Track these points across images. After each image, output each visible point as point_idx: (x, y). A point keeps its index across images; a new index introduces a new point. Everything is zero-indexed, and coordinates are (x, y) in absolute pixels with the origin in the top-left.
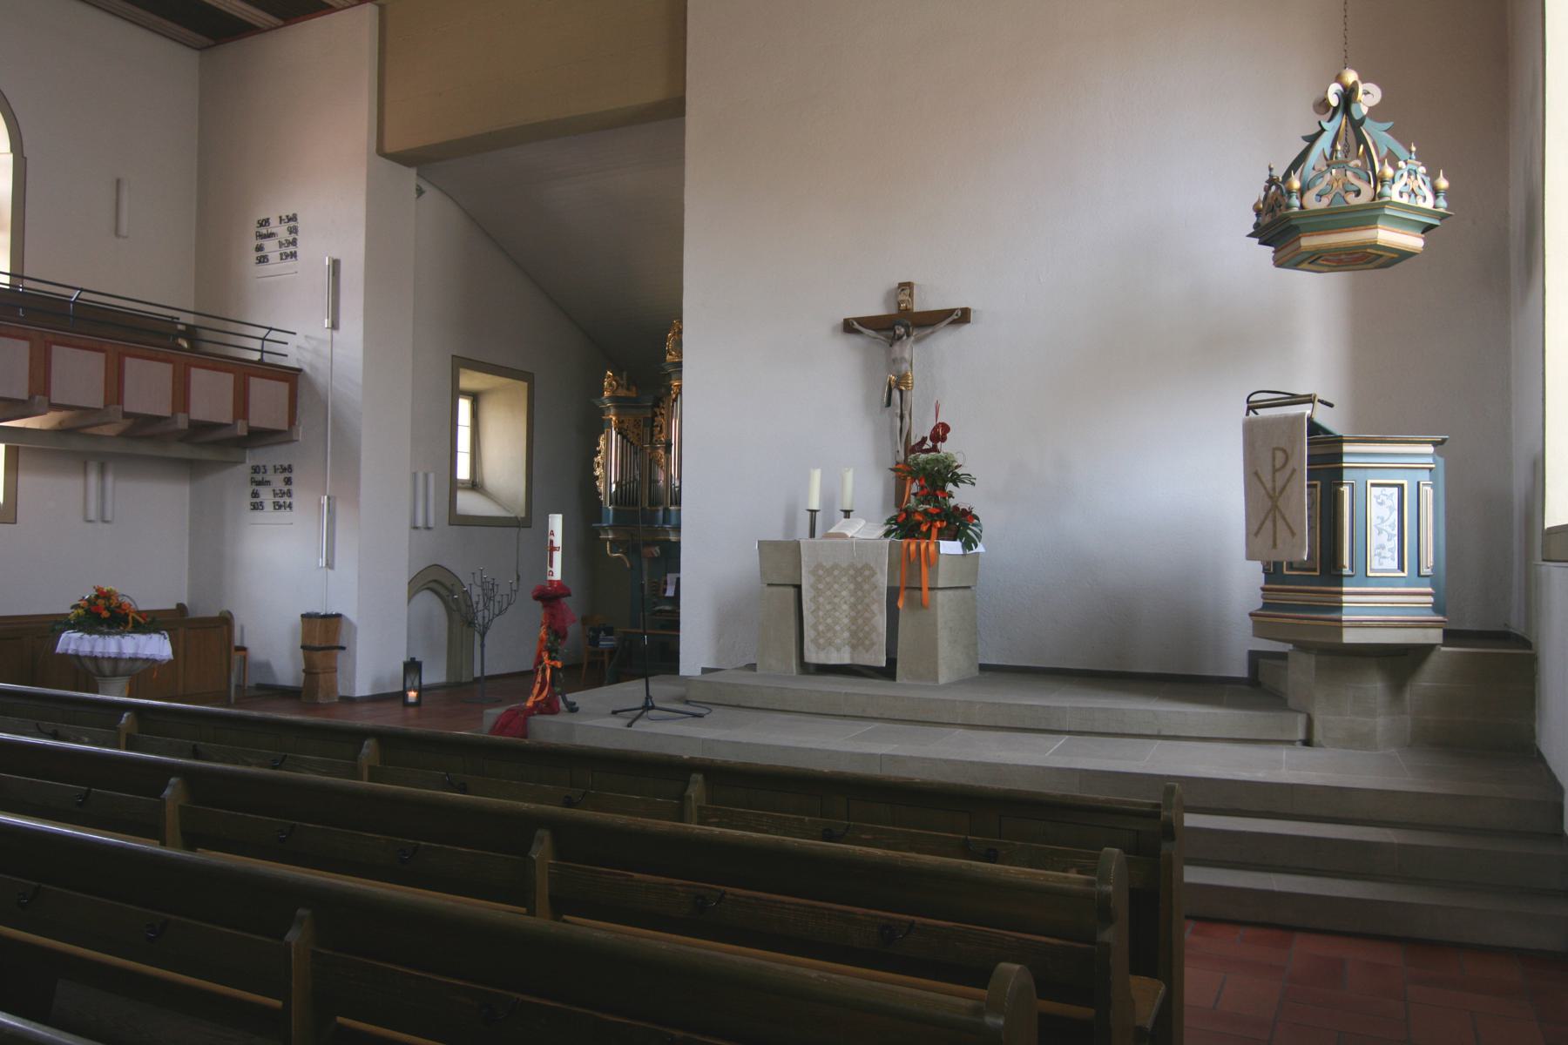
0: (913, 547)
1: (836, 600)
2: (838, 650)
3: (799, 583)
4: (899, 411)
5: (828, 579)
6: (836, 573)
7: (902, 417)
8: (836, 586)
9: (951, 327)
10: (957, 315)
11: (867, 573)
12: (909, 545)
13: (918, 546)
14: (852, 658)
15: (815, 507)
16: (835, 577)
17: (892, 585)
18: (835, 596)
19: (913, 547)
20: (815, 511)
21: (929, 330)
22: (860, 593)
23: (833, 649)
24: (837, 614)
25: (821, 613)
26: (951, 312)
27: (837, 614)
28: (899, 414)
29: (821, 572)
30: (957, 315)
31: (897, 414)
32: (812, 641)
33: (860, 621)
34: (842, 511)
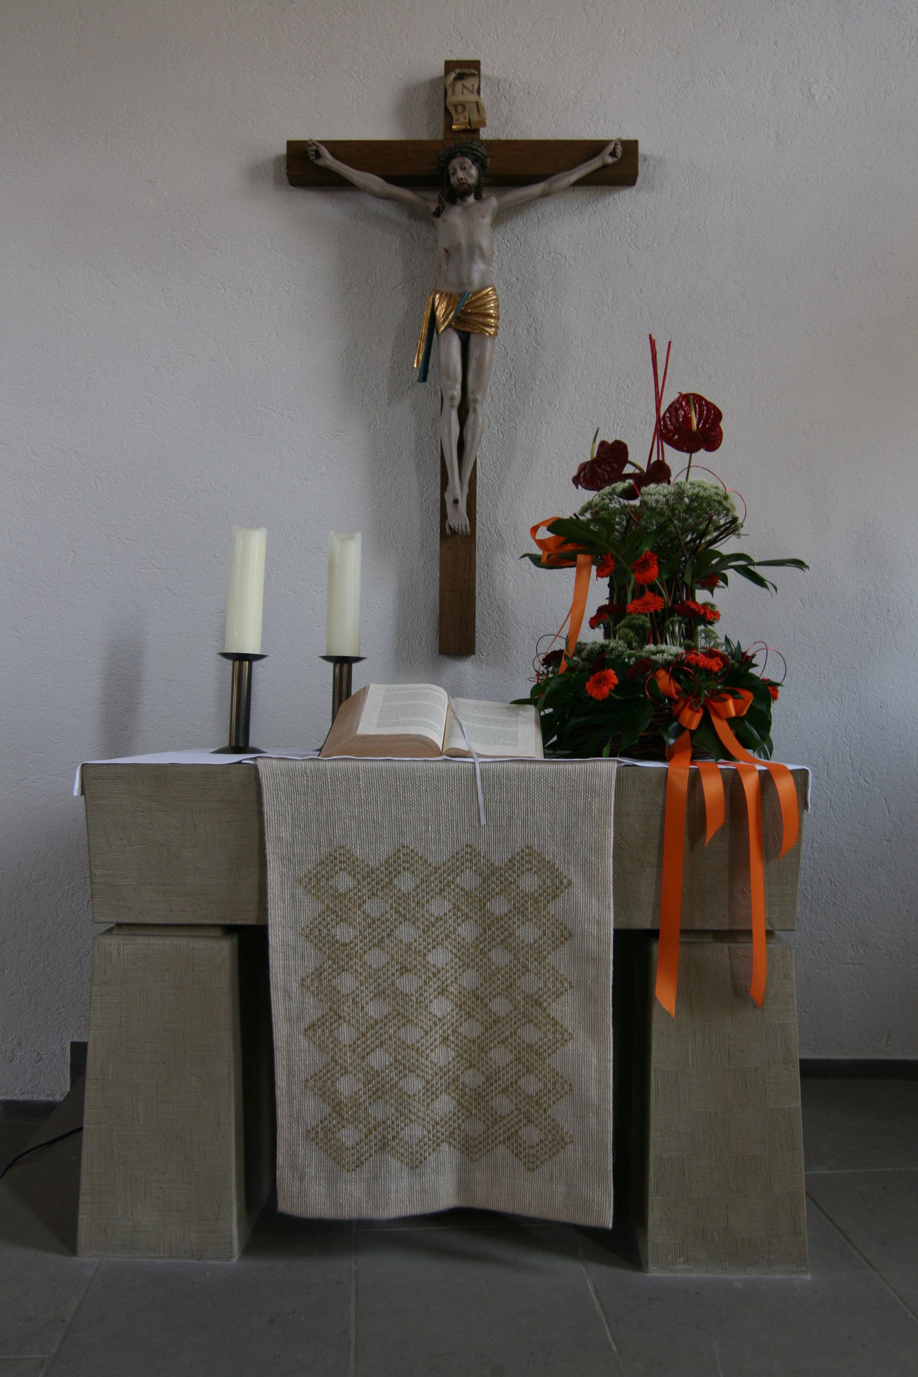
0: (713, 787)
1: (408, 984)
2: (415, 1164)
3: (250, 920)
4: (457, 392)
5: (373, 908)
6: (405, 883)
7: (464, 411)
8: (406, 933)
9: (582, 194)
10: (613, 154)
11: (529, 883)
12: (695, 780)
13: (733, 784)
14: (463, 1185)
15: (251, 646)
16: (405, 898)
17: (622, 926)
18: (404, 970)
19: (713, 787)
20: (251, 658)
21: (537, 189)
22: (499, 957)
23: (395, 1164)
24: (412, 1035)
25: (346, 1034)
26: (595, 148)
27: (412, 1035)
28: (457, 402)
29: (344, 882)
30: (613, 154)
31: (452, 398)
32: (310, 1135)
33: (500, 1056)
34: (328, 658)
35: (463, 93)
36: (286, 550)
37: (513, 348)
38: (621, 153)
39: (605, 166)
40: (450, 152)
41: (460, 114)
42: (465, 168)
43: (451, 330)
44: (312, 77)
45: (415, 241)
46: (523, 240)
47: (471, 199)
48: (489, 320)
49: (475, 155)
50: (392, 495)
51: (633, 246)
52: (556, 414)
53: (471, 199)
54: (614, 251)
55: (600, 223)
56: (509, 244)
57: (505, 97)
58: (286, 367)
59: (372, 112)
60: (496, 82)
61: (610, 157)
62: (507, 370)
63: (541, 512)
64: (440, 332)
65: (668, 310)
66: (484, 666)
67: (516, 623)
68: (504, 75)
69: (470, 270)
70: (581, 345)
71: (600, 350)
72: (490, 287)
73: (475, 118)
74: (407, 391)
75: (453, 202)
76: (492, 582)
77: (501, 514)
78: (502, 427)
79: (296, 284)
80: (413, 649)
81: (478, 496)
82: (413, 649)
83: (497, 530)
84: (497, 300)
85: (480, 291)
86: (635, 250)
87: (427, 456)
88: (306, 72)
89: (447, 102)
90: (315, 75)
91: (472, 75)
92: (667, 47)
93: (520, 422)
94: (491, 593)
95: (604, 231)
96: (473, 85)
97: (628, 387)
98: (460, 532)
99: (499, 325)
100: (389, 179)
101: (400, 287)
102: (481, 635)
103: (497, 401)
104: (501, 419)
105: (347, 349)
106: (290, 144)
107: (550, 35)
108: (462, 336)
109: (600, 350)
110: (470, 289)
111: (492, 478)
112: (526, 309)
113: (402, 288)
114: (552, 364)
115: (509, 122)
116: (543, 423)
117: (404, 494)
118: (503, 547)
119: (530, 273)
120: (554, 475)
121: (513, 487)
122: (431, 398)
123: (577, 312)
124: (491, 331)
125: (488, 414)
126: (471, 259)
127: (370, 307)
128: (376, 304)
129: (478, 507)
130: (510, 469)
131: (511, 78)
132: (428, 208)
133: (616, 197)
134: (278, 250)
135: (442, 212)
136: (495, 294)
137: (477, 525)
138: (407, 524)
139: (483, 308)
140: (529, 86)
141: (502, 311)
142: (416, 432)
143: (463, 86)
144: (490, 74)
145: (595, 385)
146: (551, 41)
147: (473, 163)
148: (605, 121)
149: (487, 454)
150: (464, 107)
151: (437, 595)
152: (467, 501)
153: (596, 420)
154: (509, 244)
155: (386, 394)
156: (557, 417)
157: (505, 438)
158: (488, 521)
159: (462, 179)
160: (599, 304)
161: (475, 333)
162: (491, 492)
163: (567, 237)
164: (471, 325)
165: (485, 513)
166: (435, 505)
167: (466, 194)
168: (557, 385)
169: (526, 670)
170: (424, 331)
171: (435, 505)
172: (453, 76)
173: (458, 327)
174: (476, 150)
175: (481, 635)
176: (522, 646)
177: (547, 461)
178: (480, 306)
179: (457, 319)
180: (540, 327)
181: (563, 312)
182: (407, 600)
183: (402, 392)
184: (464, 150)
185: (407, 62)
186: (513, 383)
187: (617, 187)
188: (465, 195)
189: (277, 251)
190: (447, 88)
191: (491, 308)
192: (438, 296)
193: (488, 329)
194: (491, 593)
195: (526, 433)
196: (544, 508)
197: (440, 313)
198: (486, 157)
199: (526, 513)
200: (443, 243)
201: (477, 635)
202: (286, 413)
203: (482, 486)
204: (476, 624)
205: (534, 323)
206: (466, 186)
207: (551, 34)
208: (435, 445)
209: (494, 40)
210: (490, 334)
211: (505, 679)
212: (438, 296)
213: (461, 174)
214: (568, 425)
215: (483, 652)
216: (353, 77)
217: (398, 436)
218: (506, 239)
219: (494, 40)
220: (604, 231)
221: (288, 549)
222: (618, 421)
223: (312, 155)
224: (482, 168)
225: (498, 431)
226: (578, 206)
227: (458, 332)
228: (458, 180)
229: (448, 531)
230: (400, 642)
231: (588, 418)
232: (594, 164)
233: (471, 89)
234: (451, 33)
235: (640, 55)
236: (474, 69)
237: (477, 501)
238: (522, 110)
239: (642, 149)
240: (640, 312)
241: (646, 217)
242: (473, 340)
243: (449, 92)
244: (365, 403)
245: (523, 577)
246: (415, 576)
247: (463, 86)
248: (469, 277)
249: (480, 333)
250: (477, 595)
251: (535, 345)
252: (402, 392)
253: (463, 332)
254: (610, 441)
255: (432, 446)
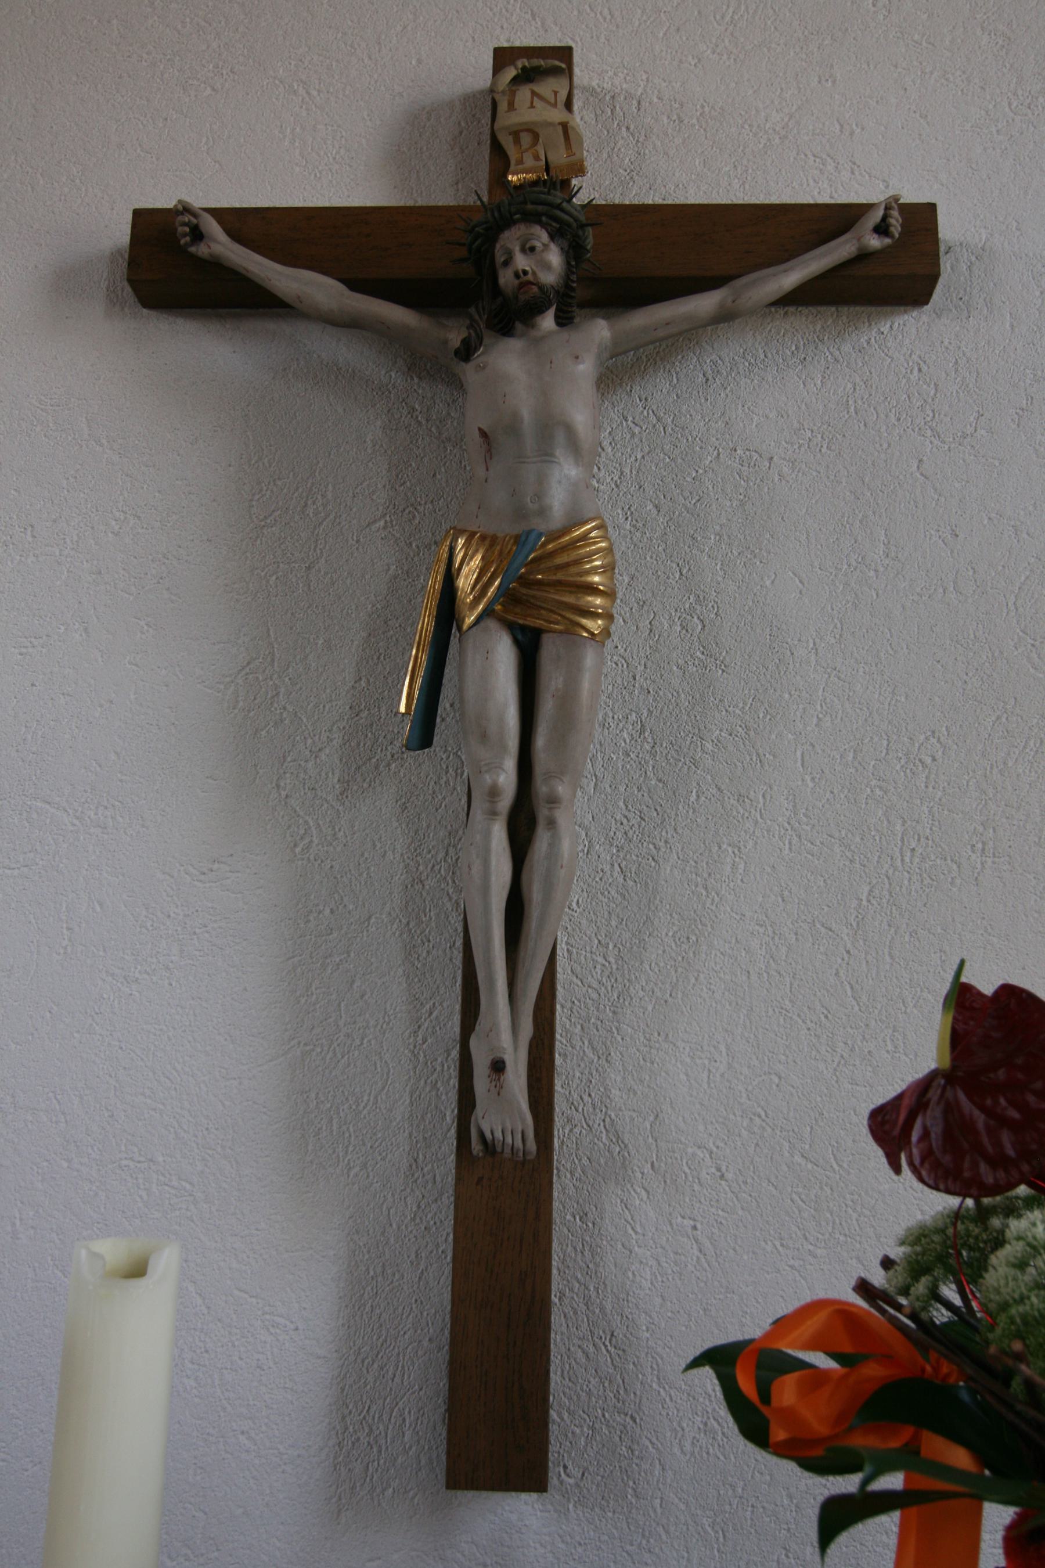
4: (507, 778)
10: (882, 229)
21: (705, 303)
28: (506, 801)
30: (882, 229)
31: (494, 793)
35: (532, 106)
36: (65, 1164)
37: (649, 663)
38: (900, 229)
39: (863, 256)
40: (496, 214)
41: (527, 150)
42: (532, 249)
43: (492, 624)
44: (209, 91)
45: (419, 423)
46: (670, 421)
47: (548, 322)
48: (590, 599)
49: (555, 219)
50: (341, 1023)
51: (929, 433)
52: (756, 823)
53: (548, 322)
54: (885, 446)
55: (850, 385)
56: (637, 430)
57: (628, 128)
58: (101, 706)
59: (334, 159)
60: (608, 98)
61: (876, 236)
62: (633, 717)
63: (722, 1076)
64: (465, 627)
65: (1023, 578)
66: (571, 1506)
67: (659, 1384)
68: (624, 86)
69: (542, 480)
70: (813, 658)
71: (861, 670)
72: (592, 519)
73: (559, 157)
74: (389, 765)
75: (506, 330)
76: (597, 1265)
77: (619, 1079)
78: (621, 855)
79: (139, 518)
80: (380, 1452)
81: (559, 1029)
82: (380, 1452)
83: (608, 1120)
84: (609, 550)
85: (566, 530)
86: (936, 442)
87: (433, 924)
88: (195, 82)
89: (496, 127)
90: (213, 89)
91: (555, 71)
92: (983, 29)
93: (666, 842)
94: (593, 1295)
95: (860, 402)
96: (556, 93)
97: (934, 759)
98: (507, 1150)
99: (614, 611)
100: (355, 285)
101: (382, 523)
102: (566, 1416)
103: (608, 790)
104: (619, 835)
105: (249, 663)
106: (140, 217)
107: (725, 7)
108: (520, 637)
109: (861, 670)
110: (541, 525)
111: (595, 985)
112: (677, 575)
113: (385, 528)
114: (745, 703)
115: (636, 178)
116: (724, 846)
117: (372, 1023)
118: (624, 1166)
119: (687, 494)
120: (754, 977)
121: (650, 1008)
122: (447, 782)
123: (801, 582)
124: (595, 625)
125: (586, 823)
126: (546, 455)
127: (309, 568)
128: (323, 560)
129: (558, 1060)
130: (642, 963)
131: (640, 90)
132: (446, 342)
133: (885, 329)
134: (104, 441)
135: (476, 349)
136: (605, 538)
137: (557, 1109)
138: (376, 1102)
139: (573, 570)
140: (682, 105)
141: (622, 581)
142: (407, 866)
143: (534, 93)
144: (594, 84)
145: (851, 755)
146: (728, 18)
147: (552, 237)
148: (853, 173)
149: (584, 921)
150: (536, 137)
151: (447, 1296)
152: (530, 1053)
153: (858, 839)
154: (637, 430)
155: (337, 771)
156: (758, 833)
157: (630, 883)
158: (586, 1098)
159: (525, 273)
160: (854, 563)
161: (554, 631)
162: (593, 1020)
163: (772, 415)
164: (543, 612)
165: (578, 1074)
166: (448, 1052)
167: (535, 309)
168: (758, 754)
169: (686, 1524)
170: (426, 623)
171: (448, 1052)
172: (511, 73)
173: (510, 617)
174: (559, 207)
175: (566, 1416)
176: (676, 1450)
177: (737, 941)
178: (568, 565)
179: (509, 597)
180: (713, 616)
181: (768, 583)
182: (368, 1308)
183: (377, 768)
184: (530, 207)
185: (414, 62)
186: (648, 747)
187: (889, 309)
188: (532, 310)
189: (101, 445)
190: (497, 97)
191: (594, 571)
192: (461, 542)
193: (585, 622)
194: (593, 1295)
195: (683, 871)
196: (730, 1066)
197: (465, 581)
198: (582, 226)
199: (683, 1077)
200: (478, 417)
201: (553, 1414)
202: (92, 814)
203: (569, 1005)
204: (552, 1385)
205: (698, 607)
206: (535, 289)
207: (728, 6)
208: (455, 897)
209: (605, 19)
210: (593, 634)
211: (628, 1548)
212: (461, 542)
213: (521, 262)
214: (787, 852)
215: (570, 1467)
216: (295, 92)
217: (361, 875)
218: (630, 419)
219: (605, 19)
220: (860, 402)
221: (69, 1161)
222: (913, 845)
223: (185, 235)
224: (574, 252)
225: (612, 865)
226: (797, 348)
227: (512, 628)
228: (517, 275)
229: (476, 1147)
230: (346, 1428)
231: (837, 835)
232: (841, 250)
233: (553, 101)
234: (510, 7)
235: (924, 44)
236: (561, 61)
237: (558, 1045)
238: (666, 154)
239: (947, 229)
240: (955, 583)
241: (956, 370)
242: (550, 649)
243: (503, 106)
244: (283, 793)
245: (676, 1253)
246: (392, 1240)
247: (534, 93)
248: (539, 495)
249: (566, 632)
250: (555, 1299)
251: (703, 657)
252: (377, 768)
253: (523, 628)
254: (987, 988)
255: (446, 899)
